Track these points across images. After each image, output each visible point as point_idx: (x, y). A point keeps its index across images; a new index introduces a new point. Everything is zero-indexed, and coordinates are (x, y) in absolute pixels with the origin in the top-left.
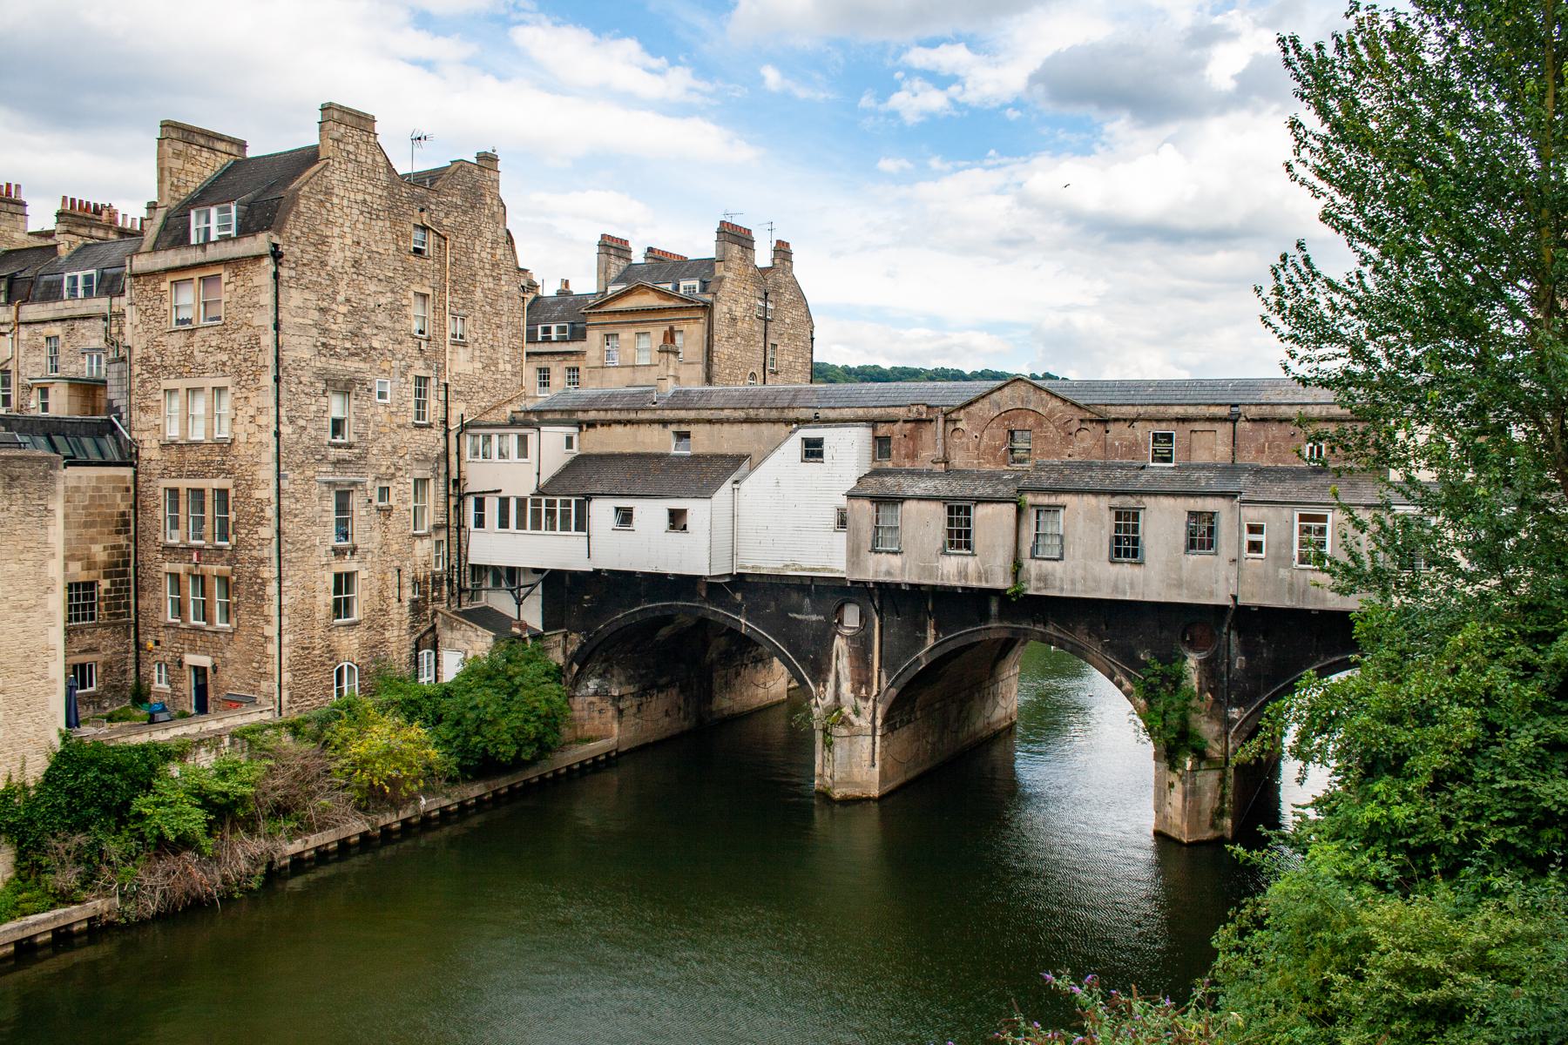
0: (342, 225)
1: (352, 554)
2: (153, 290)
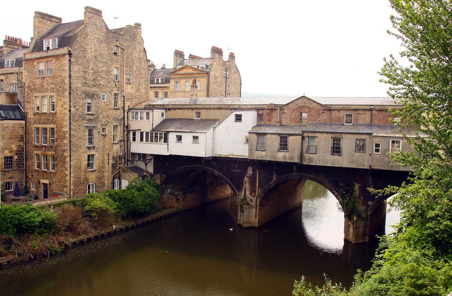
0: (91, 45)
1: (93, 149)
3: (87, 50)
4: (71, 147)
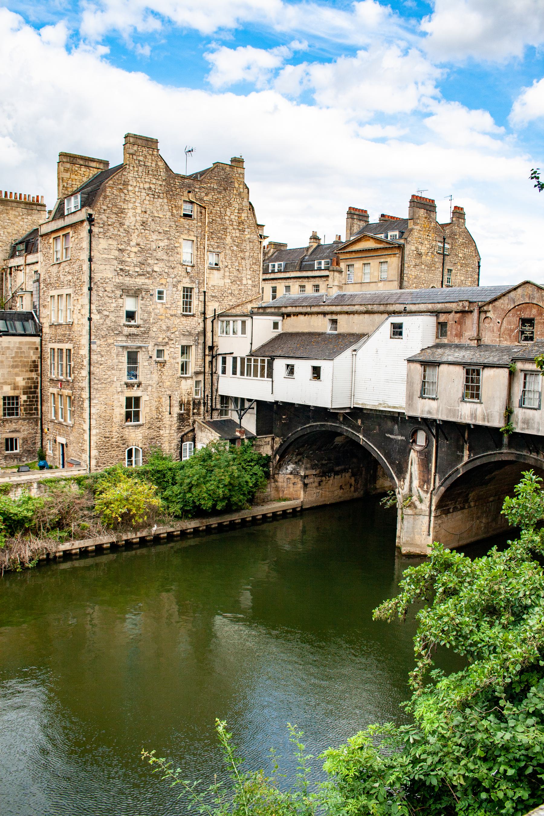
0: (135, 202)
1: (138, 386)
2: (47, 243)
3: (126, 211)
4: (92, 383)
